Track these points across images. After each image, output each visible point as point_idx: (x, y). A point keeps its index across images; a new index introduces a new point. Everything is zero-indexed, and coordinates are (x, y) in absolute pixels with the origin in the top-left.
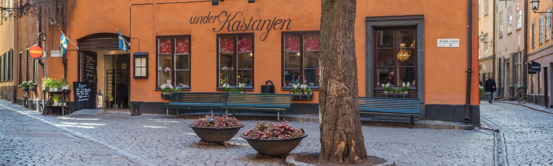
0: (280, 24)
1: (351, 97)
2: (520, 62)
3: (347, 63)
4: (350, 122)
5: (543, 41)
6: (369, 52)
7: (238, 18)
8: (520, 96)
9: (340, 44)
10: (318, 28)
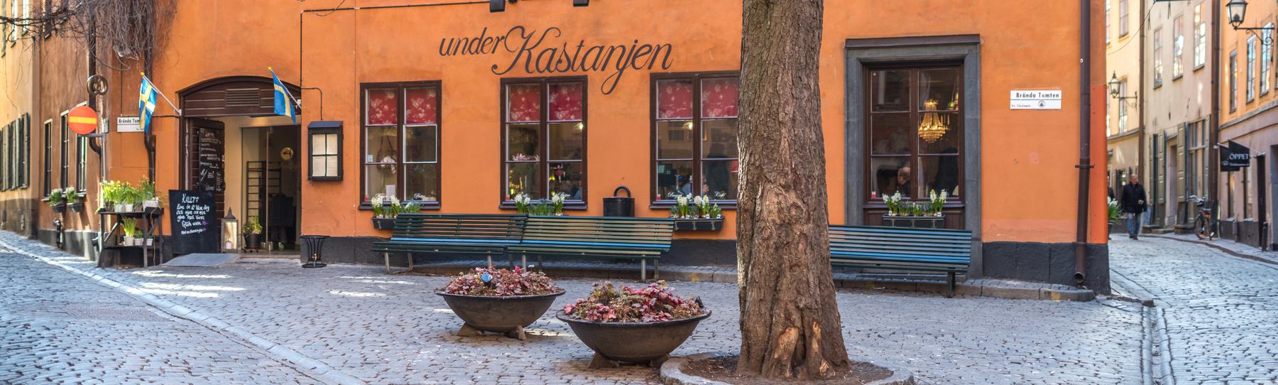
0: (647, 56)
1: (811, 225)
2: (1201, 143)
3: (802, 147)
4: (808, 283)
5: (1254, 94)
6: (853, 120)
7: (550, 42)
8: (1202, 222)
9: (786, 103)
10: (734, 65)
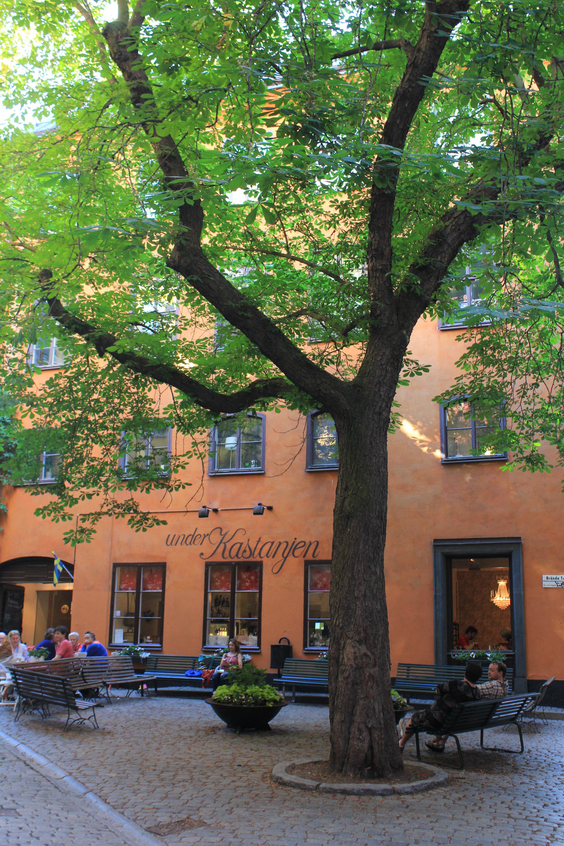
0: (302, 549)
1: (376, 669)
4: (374, 709)
6: (440, 594)
7: (239, 538)
9: (360, 584)
10: (330, 558)
